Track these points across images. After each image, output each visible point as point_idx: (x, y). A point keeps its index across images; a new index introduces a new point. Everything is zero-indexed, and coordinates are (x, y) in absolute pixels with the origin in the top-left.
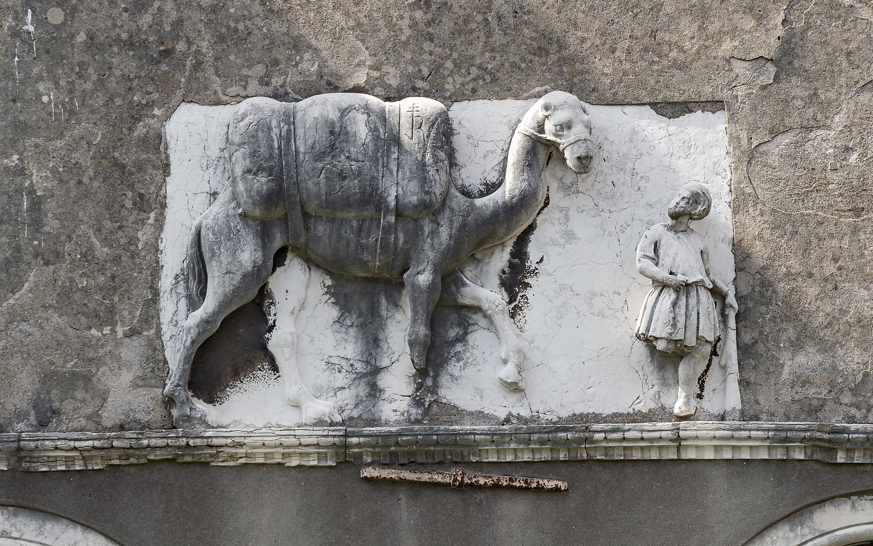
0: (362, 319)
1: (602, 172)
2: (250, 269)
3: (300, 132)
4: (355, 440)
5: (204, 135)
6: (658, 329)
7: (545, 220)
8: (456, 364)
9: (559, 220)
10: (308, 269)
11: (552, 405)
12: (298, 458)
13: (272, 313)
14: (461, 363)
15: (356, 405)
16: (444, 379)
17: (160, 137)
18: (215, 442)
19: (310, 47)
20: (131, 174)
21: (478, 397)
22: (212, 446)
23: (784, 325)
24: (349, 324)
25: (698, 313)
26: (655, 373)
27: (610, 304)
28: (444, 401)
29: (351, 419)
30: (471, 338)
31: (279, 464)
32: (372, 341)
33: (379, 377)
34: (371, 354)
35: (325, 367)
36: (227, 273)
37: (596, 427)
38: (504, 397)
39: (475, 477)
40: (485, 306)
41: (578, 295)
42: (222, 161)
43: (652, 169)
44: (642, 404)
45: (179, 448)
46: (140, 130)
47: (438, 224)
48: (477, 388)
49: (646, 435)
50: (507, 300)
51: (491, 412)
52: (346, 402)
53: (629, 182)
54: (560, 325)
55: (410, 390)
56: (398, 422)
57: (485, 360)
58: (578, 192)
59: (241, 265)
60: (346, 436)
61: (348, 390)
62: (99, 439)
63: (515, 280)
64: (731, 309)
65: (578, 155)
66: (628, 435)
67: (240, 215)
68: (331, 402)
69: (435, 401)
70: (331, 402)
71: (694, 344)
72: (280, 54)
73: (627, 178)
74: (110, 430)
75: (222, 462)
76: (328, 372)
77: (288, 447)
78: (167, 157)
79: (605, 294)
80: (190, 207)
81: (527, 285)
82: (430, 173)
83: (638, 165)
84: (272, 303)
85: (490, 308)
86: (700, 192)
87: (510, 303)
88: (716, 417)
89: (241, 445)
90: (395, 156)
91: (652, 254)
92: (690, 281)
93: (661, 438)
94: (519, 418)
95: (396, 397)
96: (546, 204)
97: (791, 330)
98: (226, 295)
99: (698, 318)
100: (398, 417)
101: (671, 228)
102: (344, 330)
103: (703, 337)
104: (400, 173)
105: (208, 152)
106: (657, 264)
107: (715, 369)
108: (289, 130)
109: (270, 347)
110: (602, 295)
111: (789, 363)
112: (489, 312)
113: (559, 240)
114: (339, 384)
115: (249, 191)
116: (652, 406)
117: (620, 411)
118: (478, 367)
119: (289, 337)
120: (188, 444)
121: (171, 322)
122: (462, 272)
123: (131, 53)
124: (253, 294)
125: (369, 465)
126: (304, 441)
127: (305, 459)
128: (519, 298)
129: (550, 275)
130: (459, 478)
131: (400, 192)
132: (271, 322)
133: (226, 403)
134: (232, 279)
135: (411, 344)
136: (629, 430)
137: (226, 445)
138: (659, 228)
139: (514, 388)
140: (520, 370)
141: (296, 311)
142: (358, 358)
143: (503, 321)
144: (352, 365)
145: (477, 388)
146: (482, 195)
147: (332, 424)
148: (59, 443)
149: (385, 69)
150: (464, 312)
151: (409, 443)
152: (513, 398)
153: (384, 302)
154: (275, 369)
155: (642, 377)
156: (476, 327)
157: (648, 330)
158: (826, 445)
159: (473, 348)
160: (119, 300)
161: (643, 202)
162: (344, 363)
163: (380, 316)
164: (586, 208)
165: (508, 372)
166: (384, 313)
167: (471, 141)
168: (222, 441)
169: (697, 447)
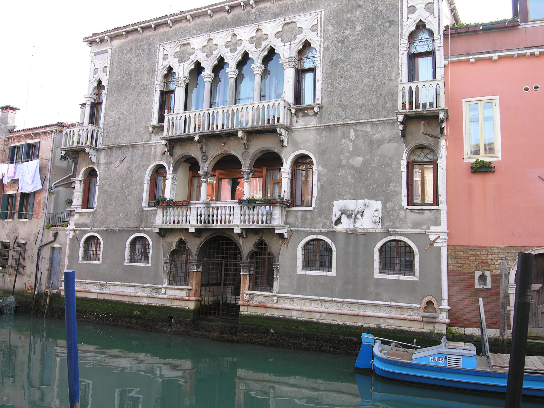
48: (358, 225)
63: (362, 216)
138: (374, 211)
145: (358, 225)
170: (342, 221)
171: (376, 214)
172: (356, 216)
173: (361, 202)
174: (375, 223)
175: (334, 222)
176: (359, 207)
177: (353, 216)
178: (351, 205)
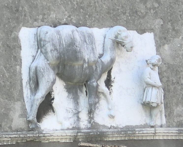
0: (74, 96)
2: (53, 81)
3: (63, 38)
13: (53, 94)
14: (99, 110)
15: (74, 123)
16: (95, 115)
17: (18, 37)
20: (12, 49)
24: (71, 97)
28: (96, 122)
29: (73, 127)
30: (100, 102)
32: (77, 103)
34: (77, 107)
37: (137, 130)
42: (34, 46)
45: (36, 137)
46: (13, 36)
47: (97, 67)
49: (148, 132)
58: (121, 57)
59: (51, 79)
60: (77, 133)
62: (16, 134)
63: (108, 83)
65: (131, 46)
66: (144, 132)
72: (46, 12)
74: (14, 131)
81: (112, 86)
84: (52, 91)
93: (172, 133)
94: (113, 127)
97: (175, 100)
98: (47, 89)
100: (85, 127)
102: (69, 99)
108: (60, 37)
110: (130, 89)
111: (175, 110)
115: (52, 56)
121: (26, 97)
123: (8, 10)
131: (89, 57)
133: (43, 123)
137: (48, 136)
142: (74, 108)
148: (7, 136)
149: (71, 17)
152: (112, 120)
153: (79, 91)
154: (54, 112)
157: (150, 100)
160: (13, 90)
162: (70, 110)
163: (78, 95)
166: (79, 94)
169: (158, 135)
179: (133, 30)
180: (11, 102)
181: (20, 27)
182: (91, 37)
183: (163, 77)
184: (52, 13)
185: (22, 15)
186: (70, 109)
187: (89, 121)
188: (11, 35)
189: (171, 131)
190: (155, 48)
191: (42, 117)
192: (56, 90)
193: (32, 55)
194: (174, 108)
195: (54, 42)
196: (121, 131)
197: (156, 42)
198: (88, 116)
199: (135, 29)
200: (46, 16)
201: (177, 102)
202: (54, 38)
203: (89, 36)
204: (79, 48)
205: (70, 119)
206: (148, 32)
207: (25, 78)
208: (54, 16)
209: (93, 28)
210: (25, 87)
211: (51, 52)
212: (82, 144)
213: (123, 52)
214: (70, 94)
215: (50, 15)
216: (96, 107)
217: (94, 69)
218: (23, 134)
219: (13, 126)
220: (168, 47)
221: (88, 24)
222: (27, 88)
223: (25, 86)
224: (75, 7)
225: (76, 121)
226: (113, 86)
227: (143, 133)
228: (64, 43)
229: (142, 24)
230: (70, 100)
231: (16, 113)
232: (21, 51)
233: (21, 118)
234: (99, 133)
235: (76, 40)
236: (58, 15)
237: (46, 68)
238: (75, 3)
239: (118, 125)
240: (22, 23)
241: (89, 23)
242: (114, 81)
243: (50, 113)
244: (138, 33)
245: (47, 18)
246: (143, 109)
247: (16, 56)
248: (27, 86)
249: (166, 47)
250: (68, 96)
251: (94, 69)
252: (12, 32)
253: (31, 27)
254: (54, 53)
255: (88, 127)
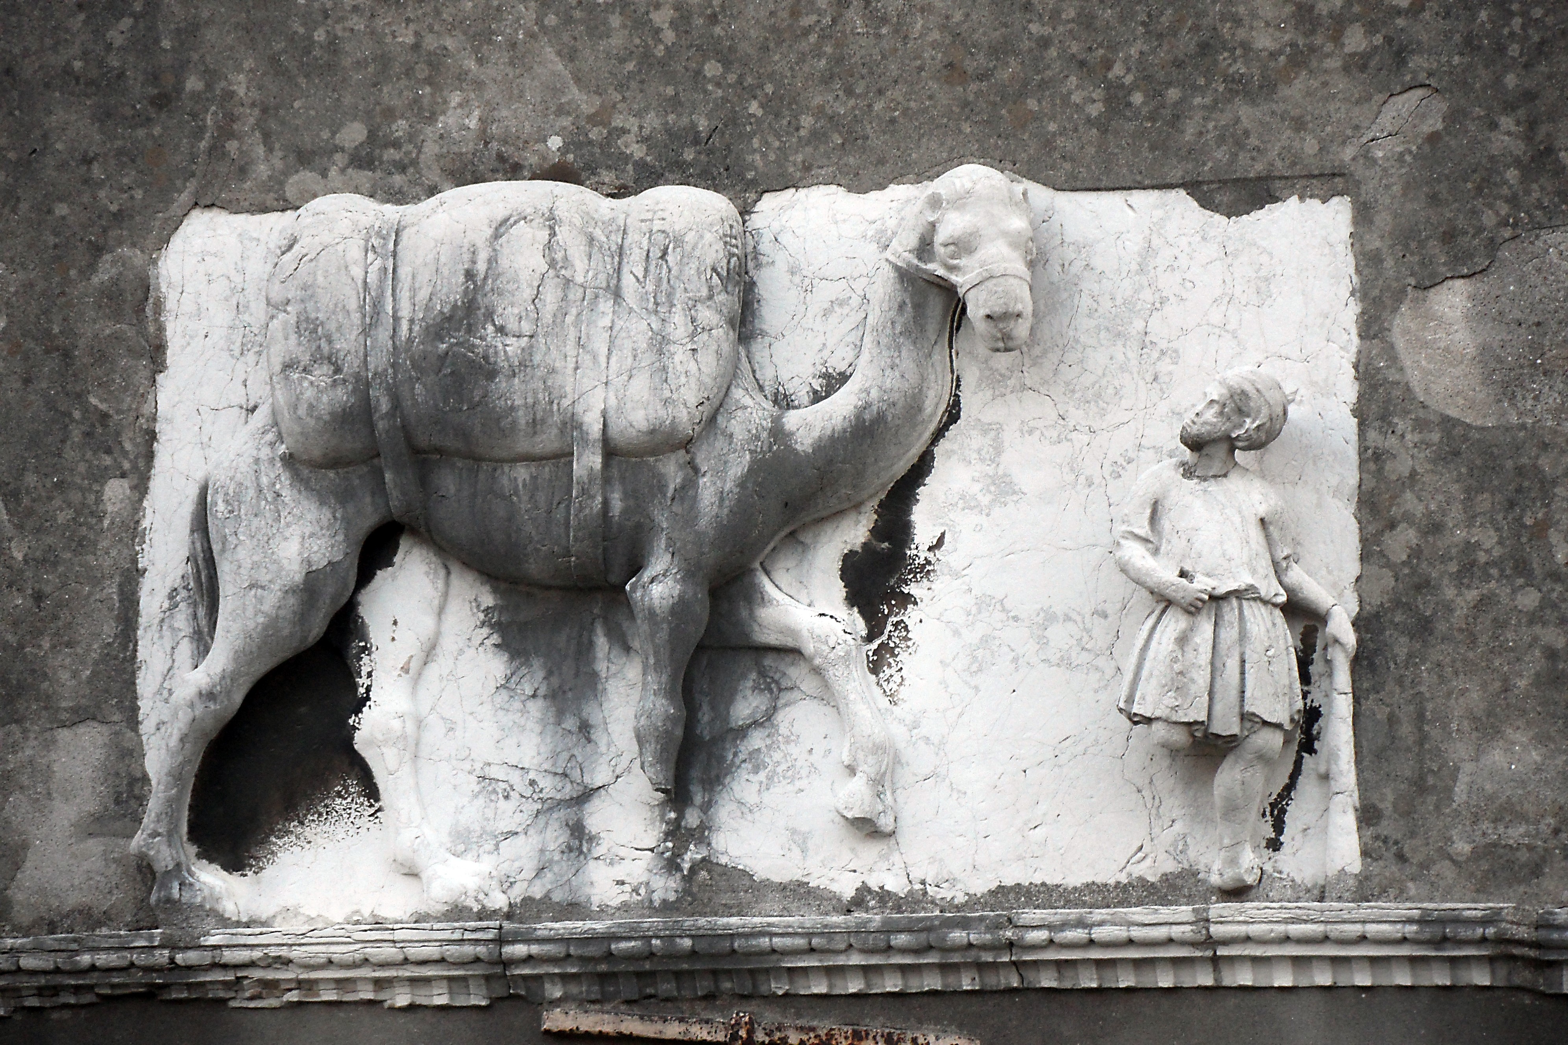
0: (555, 681)
1: (1077, 341)
4: (520, 950)
5: (238, 279)
6: (1149, 699)
7: (949, 454)
8: (751, 777)
9: (979, 452)
10: (442, 573)
11: (955, 866)
12: (407, 989)
13: (364, 671)
14: (762, 776)
16: (725, 812)
18: (228, 956)
19: (461, 77)
21: (796, 851)
22: (225, 967)
23: (1458, 683)
24: (529, 691)
25: (1243, 662)
26: (1177, 792)
27: (1086, 638)
28: (723, 860)
29: (528, 901)
30: (783, 718)
31: (370, 1002)
33: (589, 807)
35: (477, 788)
36: (251, 586)
38: (853, 850)
39: (779, 1029)
40: (809, 648)
41: (1016, 619)
43: (1184, 332)
44: (1148, 862)
46: (104, 273)
47: (696, 470)
48: (788, 826)
49: (1137, 933)
50: (864, 633)
51: (823, 883)
52: (517, 864)
53: (1134, 362)
54: (977, 688)
55: (651, 836)
56: (625, 907)
57: (813, 768)
59: (281, 568)
60: (501, 940)
61: (522, 837)
63: (879, 582)
64: (1338, 648)
66: (1098, 933)
67: (283, 458)
68: (487, 864)
69: (703, 859)
70: (487, 864)
71: (1235, 730)
73: (1130, 354)
75: (252, 998)
76: (481, 801)
77: (383, 965)
78: (161, 329)
79: (1074, 616)
80: (205, 440)
81: (907, 600)
82: (677, 359)
83: (1155, 324)
84: (365, 648)
85: (817, 653)
86: (1248, 387)
87: (869, 639)
88: (1308, 891)
89: (287, 962)
90: (606, 321)
91: (1144, 530)
92: (1222, 590)
94: (884, 896)
95: (622, 852)
96: (953, 414)
99: (1243, 673)
100: (625, 897)
101: (1188, 472)
102: (517, 705)
103: (1254, 714)
104: (613, 359)
105: (246, 318)
106: (1156, 552)
107: (1307, 785)
109: (360, 741)
110: (1068, 618)
112: (817, 661)
113: (980, 496)
114: (504, 825)
116: (1170, 866)
117: (1099, 880)
118: (798, 784)
119: (396, 724)
120: (172, 960)
121: (159, 692)
122: (768, 573)
124: (317, 627)
125: (555, 1003)
126: (415, 952)
127: (423, 992)
128: (889, 627)
129: (956, 575)
130: (743, 1033)
132: (362, 690)
133: (269, 872)
134: (260, 600)
135: (641, 740)
136: (1101, 924)
138: (1159, 468)
139: (867, 828)
140: (878, 784)
141: (414, 665)
142: (547, 766)
143: (855, 683)
144: (532, 783)
146: (817, 397)
147: (484, 914)
150: (769, 661)
151: (630, 957)
152: (871, 851)
153: (601, 642)
154: (372, 792)
155: (1148, 799)
156: (796, 695)
158: (1532, 953)
159: (788, 741)
161: (1163, 407)
162: (515, 777)
164: (1040, 424)
165: (855, 795)
166: (601, 667)
167: (797, 279)
168: (243, 955)
170: (376, 728)
171: (1219, 531)
172: (727, 584)
173: (833, 239)
174: (1203, 749)
175: (164, 740)
176: (794, 352)
177: (659, 586)
178: (595, 288)
179: (1153, 187)
180: (25, 731)
181: (175, 209)
182: (669, 258)
183: (1392, 525)
184: (455, 98)
185: (202, 129)
186: (518, 772)
187: (668, 854)
188: (92, 267)
189: (1356, 929)
190: (1349, 314)
191: (272, 832)
192: (393, 639)
193: (243, 402)
194: (1459, 751)
195: (318, 310)
196: (889, 929)
197: (1368, 261)
198: (662, 816)
199: (1176, 175)
200: (400, 127)
201: (1490, 714)
202: (320, 279)
203: (656, 253)
204: (524, 341)
205: (502, 845)
206: (1302, 198)
207: (164, 557)
208: (473, 123)
209: (802, 192)
210: (155, 627)
211: (287, 378)
212: (558, 1020)
213: (1045, 352)
214: (527, 663)
215: (432, 119)
216: (741, 757)
217: (672, 487)
218: (37, 949)
219: (20, 896)
220: (1472, 297)
221: (753, 167)
222: (171, 627)
223: (157, 621)
224: (660, 51)
225: (557, 857)
226: (915, 603)
227: (1091, 943)
228: (405, 312)
229: (1239, 145)
230: (524, 711)
231: (57, 803)
232: (160, 378)
233: (91, 842)
234: (687, 943)
235: (511, 287)
236: (505, 113)
237: (252, 493)
238: (662, 17)
239: (929, 881)
240: (192, 185)
241: (764, 155)
242: (929, 563)
243: (338, 801)
244: (1206, 203)
245: (411, 137)
246: (1170, 767)
247: (104, 417)
248: (172, 616)
249: (1453, 300)
250: (508, 680)
251: (672, 487)
252: (98, 250)
253: (265, 210)
254: (306, 384)
255: (657, 897)
